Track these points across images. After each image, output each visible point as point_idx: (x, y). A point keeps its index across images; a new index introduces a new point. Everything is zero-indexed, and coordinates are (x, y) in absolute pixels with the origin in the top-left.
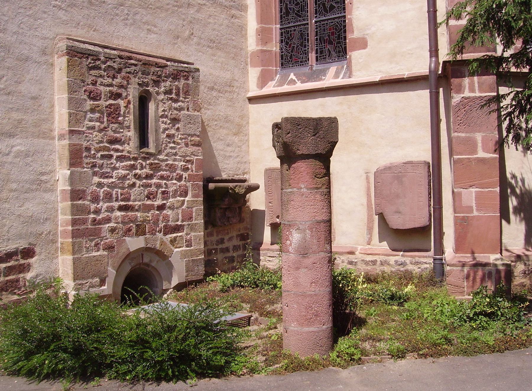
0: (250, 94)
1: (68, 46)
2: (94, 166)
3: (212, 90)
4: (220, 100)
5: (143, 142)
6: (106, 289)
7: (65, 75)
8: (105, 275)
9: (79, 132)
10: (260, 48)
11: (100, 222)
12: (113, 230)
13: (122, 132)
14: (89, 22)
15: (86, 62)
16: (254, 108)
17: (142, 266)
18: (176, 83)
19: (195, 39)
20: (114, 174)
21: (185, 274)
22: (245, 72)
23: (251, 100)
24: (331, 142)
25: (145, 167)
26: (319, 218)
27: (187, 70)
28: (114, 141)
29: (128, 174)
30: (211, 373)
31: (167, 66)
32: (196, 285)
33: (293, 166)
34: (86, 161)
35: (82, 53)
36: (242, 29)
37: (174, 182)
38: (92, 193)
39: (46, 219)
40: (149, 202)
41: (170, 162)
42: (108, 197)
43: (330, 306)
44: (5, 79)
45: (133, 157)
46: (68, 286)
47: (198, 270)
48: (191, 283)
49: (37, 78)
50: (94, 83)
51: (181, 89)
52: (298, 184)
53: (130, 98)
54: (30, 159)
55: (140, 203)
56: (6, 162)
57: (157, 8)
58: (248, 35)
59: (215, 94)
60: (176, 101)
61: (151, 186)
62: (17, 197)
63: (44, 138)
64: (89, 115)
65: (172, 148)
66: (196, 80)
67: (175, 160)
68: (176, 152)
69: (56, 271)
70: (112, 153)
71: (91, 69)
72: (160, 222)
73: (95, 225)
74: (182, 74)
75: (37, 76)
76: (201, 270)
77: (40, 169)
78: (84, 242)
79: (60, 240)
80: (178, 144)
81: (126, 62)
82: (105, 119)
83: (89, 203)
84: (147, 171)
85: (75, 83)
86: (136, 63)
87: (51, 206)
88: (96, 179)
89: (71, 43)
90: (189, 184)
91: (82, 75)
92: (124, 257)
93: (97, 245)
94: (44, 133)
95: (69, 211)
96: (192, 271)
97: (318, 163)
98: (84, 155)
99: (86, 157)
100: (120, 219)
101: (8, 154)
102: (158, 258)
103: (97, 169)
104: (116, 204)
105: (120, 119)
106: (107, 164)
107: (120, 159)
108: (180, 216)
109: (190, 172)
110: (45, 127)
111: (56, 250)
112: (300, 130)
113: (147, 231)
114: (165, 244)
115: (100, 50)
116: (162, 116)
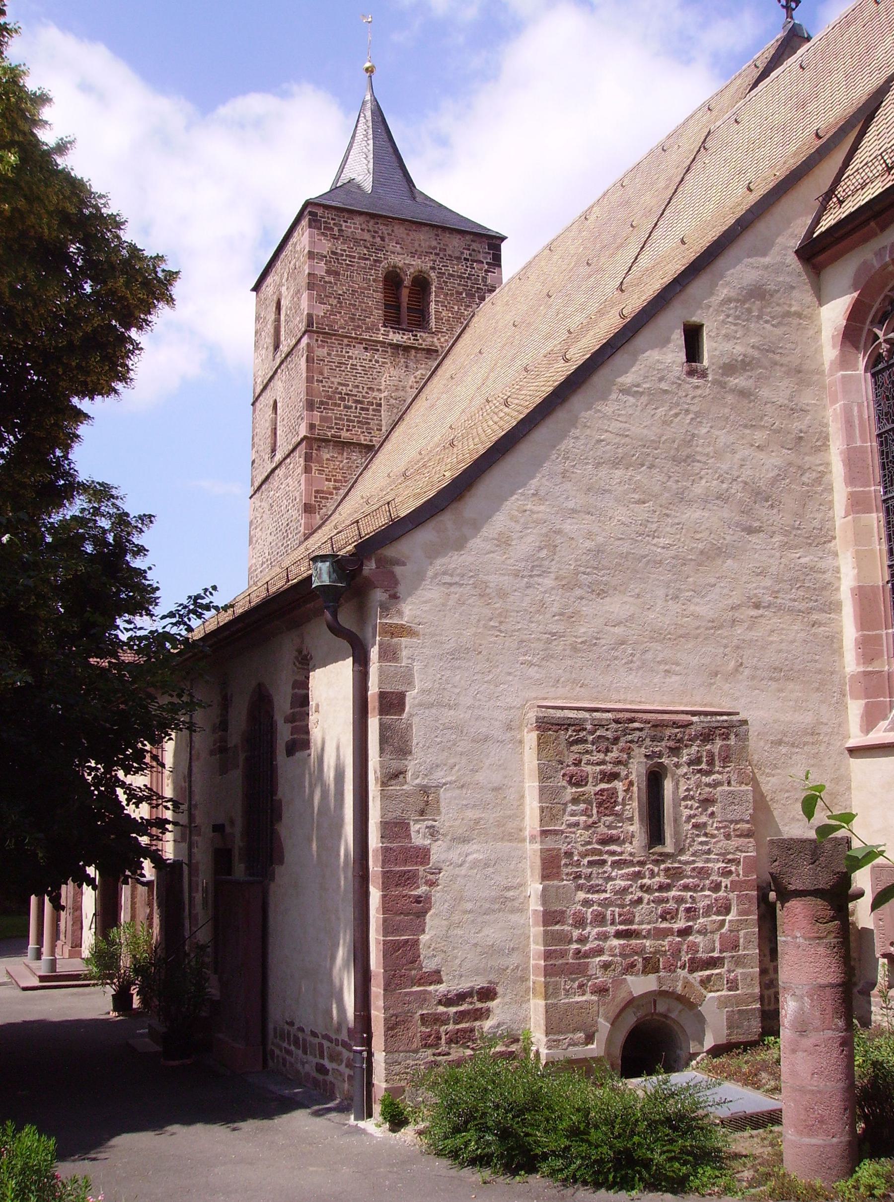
0: (852, 743)
1: (538, 718)
2: (578, 876)
3: (780, 745)
4: (794, 757)
5: (655, 835)
6: (595, 1049)
7: (535, 756)
8: (594, 1029)
9: (556, 833)
10: (862, 670)
11: (587, 955)
12: (606, 966)
13: (621, 827)
14: (574, 676)
15: (563, 736)
16: (857, 764)
17: (655, 1017)
18: (708, 747)
19: (747, 672)
20: (609, 886)
21: (726, 1032)
22: (841, 708)
23: (854, 752)
24: (838, 873)
25: (658, 874)
26: (822, 981)
27: (725, 725)
28: (606, 841)
29: (631, 886)
30: (665, 1186)
31: (692, 724)
32: (745, 1050)
33: (786, 905)
34: (569, 870)
35: (558, 725)
36: (833, 642)
37: (707, 893)
38: (574, 914)
39: (513, 949)
40: (665, 925)
41: (700, 865)
42: (600, 919)
43: (845, 1109)
44: (457, 768)
45: (638, 862)
46: (540, 1043)
47: (749, 1026)
48: (736, 1045)
49: (502, 761)
50: (577, 763)
51: (717, 754)
52: (793, 930)
53: (633, 777)
54: (491, 870)
55: (649, 927)
56: (458, 876)
57: (680, 636)
58: (845, 649)
59: (784, 750)
60: (708, 773)
61: (667, 901)
62: (473, 921)
63: (510, 841)
64: (571, 808)
65: (701, 843)
66: (743, 738)
67: (708, 861)
68: (709, 849)
69: (526, 1019)
70: (605, 857)
71: (572, 744)
72: (683, 953)
73: (580, 958)
74: (718, 732)
75: (499, 760)
76: (755, 1026)
77: (505, 882)
78: (562, 982)
79: (532, 977)
80: (713, 836)
81: (625, 726)
82: (595, 811)
83: (570, 928)
84: (661, 879)
85: (549, 766)
86: (642, 726)
87: (519, 932)
88: (581, 895)
89: (543, 713)
90: (733, 896)
91: (561, 753)
92: (623, 1004)
93: (581, 986)
94: (510, 834)
95: (541, 940)
96: (738, 1027)
97: (819, 901)
98: (563, 862)
99: (566, 865)
100: (617, 950)
101: (461, 865)
102: (680, 1006)
103: (582, 881)
104: (612, 929)
105: (617, 808)
106: (598, 873)
107: (617, 864)
108: (717, 944)
109: (734, 877)
110: (511, 826)
111: (527, 991)
112: (792, 857)
113: (661, 967)
114: (692, 985)
115: (587, 715)
116: (685, 798)
